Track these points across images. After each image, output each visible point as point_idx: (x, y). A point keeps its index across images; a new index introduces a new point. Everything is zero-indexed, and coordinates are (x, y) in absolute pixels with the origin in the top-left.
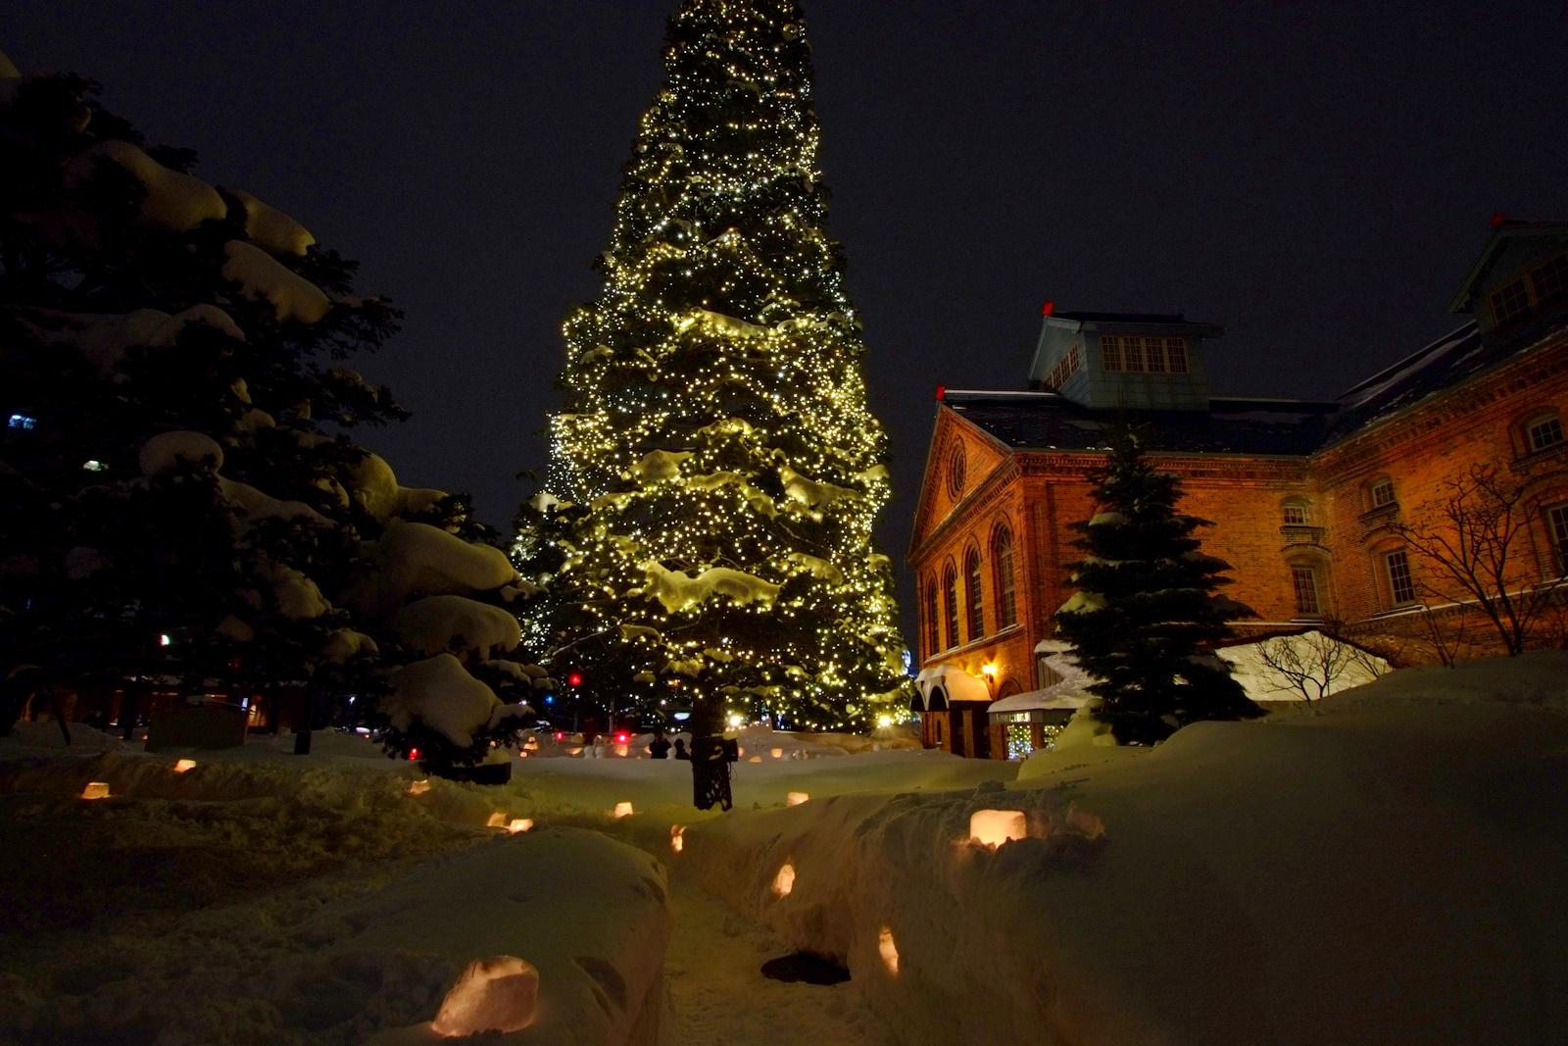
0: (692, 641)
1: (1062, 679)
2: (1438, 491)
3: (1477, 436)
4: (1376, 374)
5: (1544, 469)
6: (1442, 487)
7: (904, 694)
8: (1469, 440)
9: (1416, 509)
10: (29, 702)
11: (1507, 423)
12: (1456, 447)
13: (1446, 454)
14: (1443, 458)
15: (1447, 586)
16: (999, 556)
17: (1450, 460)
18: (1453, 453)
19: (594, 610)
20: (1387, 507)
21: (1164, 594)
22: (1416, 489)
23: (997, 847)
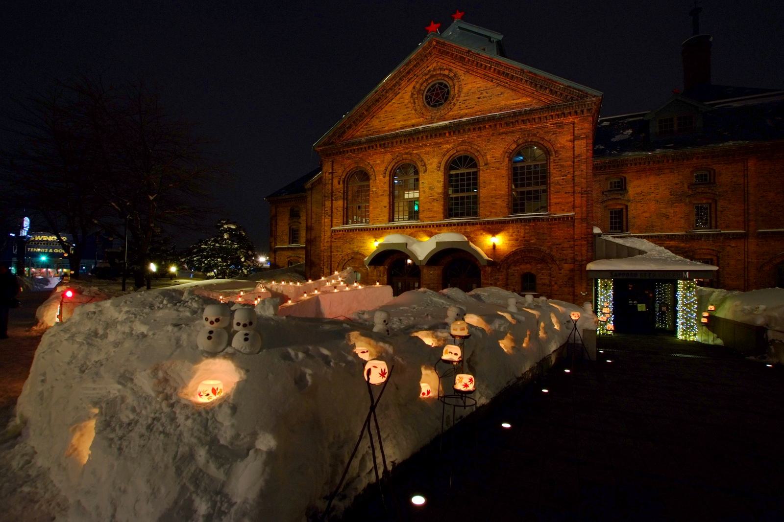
0: (21, 289)
1: (183, 293)
2: (650, 189)
3: (675, 171)
4: (606, 117)
5: (703, 190)
6: (653, 188)
7: (119, 402)
8: (671, 172)
9: (637, 194)
10: (381, 241)
11: (691, 169)
12: (664, 173)
13: (658, 175)
14: (656, 176)
15: (645, 227)
16: (453, 82)
17: (660, 178)
18: (661, 176)
19: (695, 286)
20: (621, 187)
21: (114, 202)
22: (639, 186)
23: (362, 485)
